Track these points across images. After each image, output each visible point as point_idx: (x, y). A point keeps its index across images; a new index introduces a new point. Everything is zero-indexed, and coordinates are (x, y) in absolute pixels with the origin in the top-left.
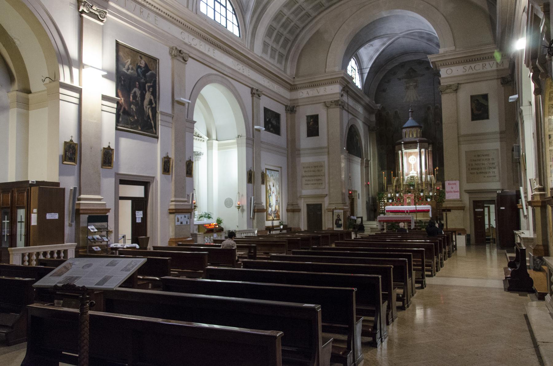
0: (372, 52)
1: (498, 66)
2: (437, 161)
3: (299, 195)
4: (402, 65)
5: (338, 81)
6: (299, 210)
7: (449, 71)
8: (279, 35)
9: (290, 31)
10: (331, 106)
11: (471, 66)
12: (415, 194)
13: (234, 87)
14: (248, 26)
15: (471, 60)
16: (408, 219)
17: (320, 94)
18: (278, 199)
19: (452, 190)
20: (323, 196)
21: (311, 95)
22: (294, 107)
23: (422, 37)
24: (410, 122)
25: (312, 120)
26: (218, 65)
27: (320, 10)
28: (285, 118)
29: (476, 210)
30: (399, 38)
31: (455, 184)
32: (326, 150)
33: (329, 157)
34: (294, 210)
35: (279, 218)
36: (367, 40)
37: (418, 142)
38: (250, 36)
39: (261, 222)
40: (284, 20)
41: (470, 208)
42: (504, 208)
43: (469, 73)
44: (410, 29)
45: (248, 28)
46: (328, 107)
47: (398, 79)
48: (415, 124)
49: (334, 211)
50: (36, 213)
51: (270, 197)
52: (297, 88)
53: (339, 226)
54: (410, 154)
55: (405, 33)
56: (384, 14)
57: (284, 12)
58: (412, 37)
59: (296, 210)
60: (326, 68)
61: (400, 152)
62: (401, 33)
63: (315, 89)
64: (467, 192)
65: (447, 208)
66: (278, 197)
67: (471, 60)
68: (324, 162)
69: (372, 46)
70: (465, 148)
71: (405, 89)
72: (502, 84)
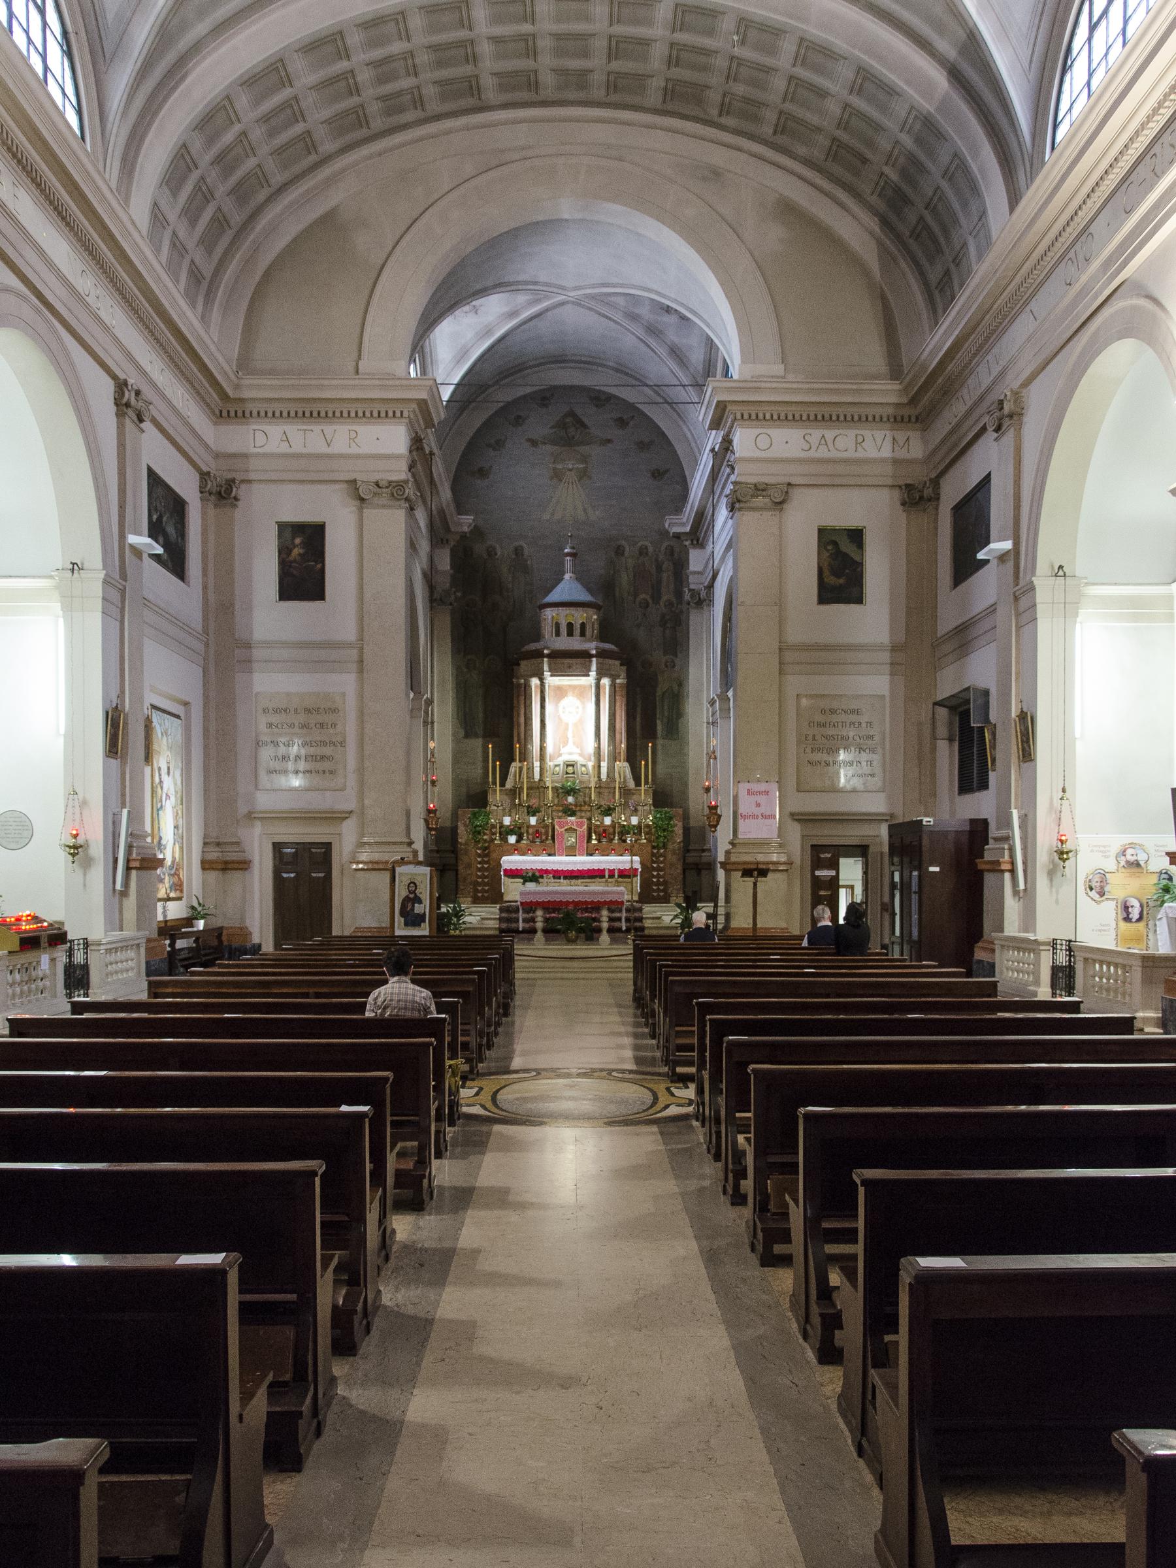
0: (469, 335)
1: (896, 448)
2: (638, 719)
3: (243, 809)
4: (545, 397)
5: (406, 414)
6: (243, 865)
7: (763, 442)
8: (203, 194)
9: (239, 184)
10: (376, 500)
11: (823, 436)
12: (590, 819)
13: (72, 365)
14: (116, 125)
15: (827, 417)
16: (615, 898)
17: (336, 452)
18: (180, 822)
19: (757, 811)
20: (336, 817)
21: (297, 447)
22: (231, 483)
23: (633, 317)
24: (568, 588)
25: (298, 541)
26: (30, 255)
27: (350, 137)
28: (199, 522)
29: (817, 873)
30: (563, 304)
31: (767, 793)
32: (354, 653)
33: (361, 681)
34: (226, 863)
35: (182, 891)
36: (478, 287)
37: (592, 656)
38: (117, 164)
39: (146, 905)
40: (228, 137)
41: (802, 867)
42: (937, 869)
43: (818, 455)
44: (614, 280)
45: (114, 132)
46: (362, 500)
47: (529, 440)
48: (584, 596)
49: (398, 870)
50: (843, 886)
51: (160, 812)
52: (248, 414)
53: (414, 920)
54: (561, 692)
55: (589, 291)
56: (567, 208)
57: (237, 106)
58: (604, 310)
59: (233, 862)
60: (360, 359)
61: (535, 682)
62: (576, 288)
63: (317, 428)
64: (796, 820)
65: (760, 866)
66: (180, 812)
67: (827, 417)
68: (344, 694)
69: (476, 313)
70: (795, 683)
71: (551, 478)
72: (903, 504)
